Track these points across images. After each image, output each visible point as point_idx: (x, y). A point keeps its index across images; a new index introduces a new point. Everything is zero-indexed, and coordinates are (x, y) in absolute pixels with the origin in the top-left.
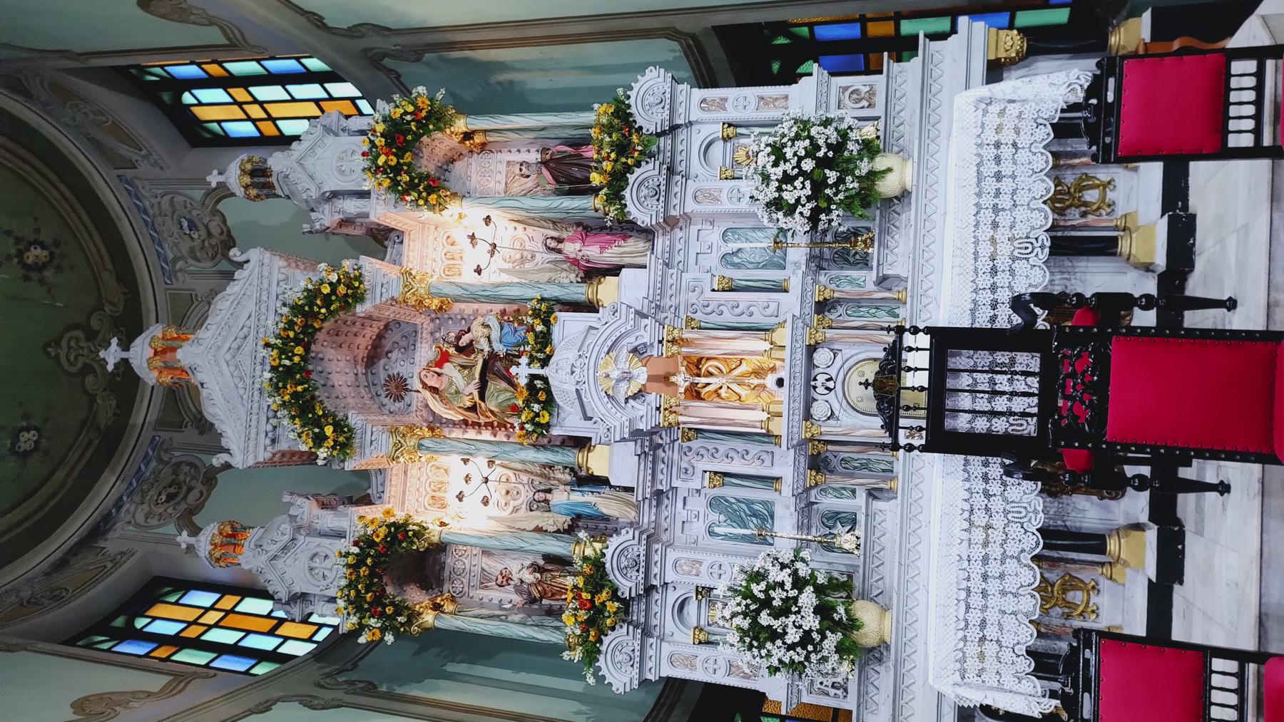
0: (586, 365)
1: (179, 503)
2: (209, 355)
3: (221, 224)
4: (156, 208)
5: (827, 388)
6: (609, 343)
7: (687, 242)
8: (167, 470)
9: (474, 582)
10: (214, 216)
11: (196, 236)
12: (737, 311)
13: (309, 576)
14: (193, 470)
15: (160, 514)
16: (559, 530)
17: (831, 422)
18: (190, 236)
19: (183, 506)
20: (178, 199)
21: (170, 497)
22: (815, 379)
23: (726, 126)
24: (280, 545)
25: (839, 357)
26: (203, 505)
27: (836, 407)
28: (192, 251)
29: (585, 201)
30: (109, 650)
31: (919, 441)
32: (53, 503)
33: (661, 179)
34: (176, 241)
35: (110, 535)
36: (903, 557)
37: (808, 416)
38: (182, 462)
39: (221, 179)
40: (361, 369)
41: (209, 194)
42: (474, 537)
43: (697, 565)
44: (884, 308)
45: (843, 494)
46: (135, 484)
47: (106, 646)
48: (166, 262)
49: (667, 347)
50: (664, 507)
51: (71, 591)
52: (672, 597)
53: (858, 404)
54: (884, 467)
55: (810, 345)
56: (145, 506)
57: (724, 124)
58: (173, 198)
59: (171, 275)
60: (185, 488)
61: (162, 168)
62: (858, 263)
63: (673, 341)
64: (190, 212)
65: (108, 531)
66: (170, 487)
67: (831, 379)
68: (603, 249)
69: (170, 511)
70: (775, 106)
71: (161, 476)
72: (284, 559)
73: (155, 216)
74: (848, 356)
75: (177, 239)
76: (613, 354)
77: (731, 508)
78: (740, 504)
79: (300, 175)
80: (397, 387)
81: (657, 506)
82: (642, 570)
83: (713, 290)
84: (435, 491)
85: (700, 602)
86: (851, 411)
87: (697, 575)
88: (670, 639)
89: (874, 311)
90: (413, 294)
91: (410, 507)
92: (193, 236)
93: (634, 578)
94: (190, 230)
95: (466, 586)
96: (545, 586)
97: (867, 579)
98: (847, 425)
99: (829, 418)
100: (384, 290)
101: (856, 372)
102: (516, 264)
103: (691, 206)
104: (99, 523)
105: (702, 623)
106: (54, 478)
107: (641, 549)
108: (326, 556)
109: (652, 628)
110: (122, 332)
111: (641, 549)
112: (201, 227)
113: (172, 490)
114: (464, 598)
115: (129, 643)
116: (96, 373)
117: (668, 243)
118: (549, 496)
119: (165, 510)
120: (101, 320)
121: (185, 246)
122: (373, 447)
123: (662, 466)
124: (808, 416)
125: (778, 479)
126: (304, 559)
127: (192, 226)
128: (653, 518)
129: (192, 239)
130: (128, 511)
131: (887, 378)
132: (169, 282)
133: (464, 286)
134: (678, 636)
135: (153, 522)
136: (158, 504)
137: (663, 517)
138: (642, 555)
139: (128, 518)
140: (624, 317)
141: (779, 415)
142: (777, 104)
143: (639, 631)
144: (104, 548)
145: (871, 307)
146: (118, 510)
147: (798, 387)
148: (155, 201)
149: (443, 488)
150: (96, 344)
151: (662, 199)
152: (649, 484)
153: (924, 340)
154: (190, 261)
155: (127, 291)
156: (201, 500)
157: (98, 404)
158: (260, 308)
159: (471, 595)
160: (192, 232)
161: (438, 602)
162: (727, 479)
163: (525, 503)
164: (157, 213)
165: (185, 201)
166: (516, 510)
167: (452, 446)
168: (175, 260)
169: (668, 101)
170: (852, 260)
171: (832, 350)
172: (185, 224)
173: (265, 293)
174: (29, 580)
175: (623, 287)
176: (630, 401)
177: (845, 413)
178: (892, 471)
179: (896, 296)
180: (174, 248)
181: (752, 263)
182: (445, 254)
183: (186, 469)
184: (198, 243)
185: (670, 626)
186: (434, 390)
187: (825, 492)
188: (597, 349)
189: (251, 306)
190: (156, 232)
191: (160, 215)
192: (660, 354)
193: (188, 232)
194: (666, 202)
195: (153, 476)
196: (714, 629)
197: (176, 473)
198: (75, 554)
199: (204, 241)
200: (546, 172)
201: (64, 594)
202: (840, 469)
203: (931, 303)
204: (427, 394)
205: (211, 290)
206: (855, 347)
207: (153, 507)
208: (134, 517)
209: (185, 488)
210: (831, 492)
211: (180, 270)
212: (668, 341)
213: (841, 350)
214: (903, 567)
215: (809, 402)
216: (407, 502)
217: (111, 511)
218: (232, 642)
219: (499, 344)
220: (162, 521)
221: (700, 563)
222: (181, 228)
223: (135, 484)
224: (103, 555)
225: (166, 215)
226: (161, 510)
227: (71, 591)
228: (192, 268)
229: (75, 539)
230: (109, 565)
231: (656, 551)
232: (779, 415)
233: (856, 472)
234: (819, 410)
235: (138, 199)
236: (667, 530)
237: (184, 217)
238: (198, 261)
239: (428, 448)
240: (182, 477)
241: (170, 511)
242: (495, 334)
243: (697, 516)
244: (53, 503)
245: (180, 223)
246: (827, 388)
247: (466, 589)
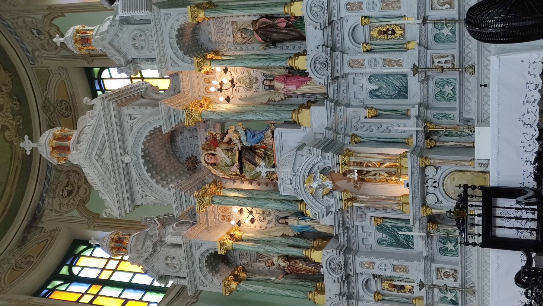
0: (298, 180)
1: (75, 196)
2: (86, 158)
3: (56, 31)
4: (15, 25)
5: (434, 187)
6: (308, 171)
7: (347, 85)
8: (62, 176)
9: (253, 259)
10: (52, 27)
11: (43, 37)
12: (382, 129)
13: (167, 268)
14: (77, 175)
15: (67, 204)
16: (295, 235)
18: (39, 37)
19: (78, 198)
20: (27, 19)
21: (70, 193)
22: (427, 182)
23: (363, 18)
24: (149, 253)
25: (439, 170)
26: (89, 196)
27: (440, 196)
28: (42, 46)
29: (284, 63)
30: (65, 291)
31: (479, 240)
32: (8, 207)
33: (328, 57)
34: (32, 41)
35: (44, 219)
36: (480, 274)
37: (424, 204)
38: (70, 171)
39: (62, 39)
40: (168, 146)
41: (46, 16)
42: (251, 247)
43: (373, 264)
46: (47, 186)
47: (63, 288)
48: (28, 52)
49: (342, 168)
50: (351, 231)
51: (35, 257)
52: (361, 279)
55: (422, 167)
56: (57, 199)
57: (362, 17)
58: (24, 19)
59: (32, 59)
60: (76, 187)
61: (14, 6)
62: (450, 100)
63: (345, 164)
64: (36, 26)
65: (41, 216)
66: (67, 186)
67: (436, 182)
68: (297, 88)
69: (71, 201)
70: (392, 7)
71: (61, 179)
72: (151, 259)
73: (16, 29)
74: (444, 170)
75: (31, 39)
76: (312, 176)
77: (389, 230)
78: (394, 228)
79: (112, 52)
80: (193, 163)
81: (347, 232)
82: (343, 269)
83: (366, 117)
84: (223, 212)
85: (376, 281)
87: (373, 269)
88: (363, 298)
90: (193, 119)
91: (211, 222)
92: (41, 38)
93: (339, 273)
94: (39, 35)
95: (249, 261)
96: (292, 267)
97: (463, 277)
99: (436, 203)
100: (176, 118)
102: (247, 85)
103: (347, 70)
104: (35, 211)
105: (379, 289)
106: (5, 193)
107: (341, 259)
108: (174, 258)
109: (352, 294)
110: (15, 99)
111: (341, 259)
112: (45, 33)
113: (69, 188)
114: (249, 267)
115: (75, 284)
116: (9, 128)
117: (336, 88)
118: (287, 221)
119: (69, 201)
120: (3, 97)
121: (38, 43)
122: (187, 204)
123: (348, 220)
124: (424, 204)
126: (162, 258)
127: (39, 32)
128: (346, 238)
129: (41, 39)
130: (48, 203)
131: (460, 210)
132: (33, 63)
133: (221, 114)
134: (366, 297)
135: (64, 209)
136: (63, 197)
137: (351, 237)
138: (342, 262)
139: (50, 207)
140: (315, 155)
141: (408, 204)
142: (393, 5)
143: (345, 298)
144: (43, 228)
146: (43, 201)
147: (417, 191)
148: (13, 21)
149: (228, 210)
150: (4, 112)
151: (329, 68)
152: (341, 225)
153: (479, 192)
154: (43, 51)
155: (11, 74)
156: (87, 194)
157: (15, 146)
158: (108, 132)
159: (253, 266)
160: (40, 36)
161: (236, 274)
162: (385, 220)
163: (274, 218)
164: (17, 27)
165: (32, 21)
166: (269, 222)
167: (230, 201)
168: (33, 51)
169: (326, 8)
170: (447, 98)
172: (35, 32)
173: (109, 124)
174: (11, 251)
175: (313, 117)
176: (325, 197)
180: (31, 44)
181: (388, 95)
182: (204, 80)
183: (73, 174)
184: (45, 41)
185: (361, 292)
186: (213, 164)
188: (303, 171)
189: (103, 130)
190: (18, 36)
191: (18, 28)
192: (338, 171)
193: (37, 36)
194: (332, 70)
195: (56, 180)
196: (385, 292)
197: (68, 177)
198: (29, 232)
199: (48, 40)
200: (256, 35)
201: (32, 260)
204: (210, 167)
205: (59, 67)
207: (61, 200)
208: (52, 206)
209: (76, 187)
211: (38, 56)
212: (342, 164)
214: (480, 279)
215: (424, 195)
216: (209, 220)
217: (39, 203)
218: (127, 280)
219: (246, 143)
220: (69, 209)
221: (374, 263)
222: (33, 34)
223: (47, 186)
224: (44, 232)
225: (22, 28)
226: (66, 202)
227: (35, 257)
228: (44, 55)
229: (25, 223)
230: (50, 239)
231: (350, 258)
232: (408, 204)
234: (431, 200)
235: (3, 20)
236: (354, 243)
237: (33, 28)
238: (47, 51)
239: (218, 203)
240: (72, 180)
241: (71, 201)
242: (243, 138)
243: (370, 235)
244: (8, 207)
245: (32, 31)
246: (434, 187)
247: (249, 263)
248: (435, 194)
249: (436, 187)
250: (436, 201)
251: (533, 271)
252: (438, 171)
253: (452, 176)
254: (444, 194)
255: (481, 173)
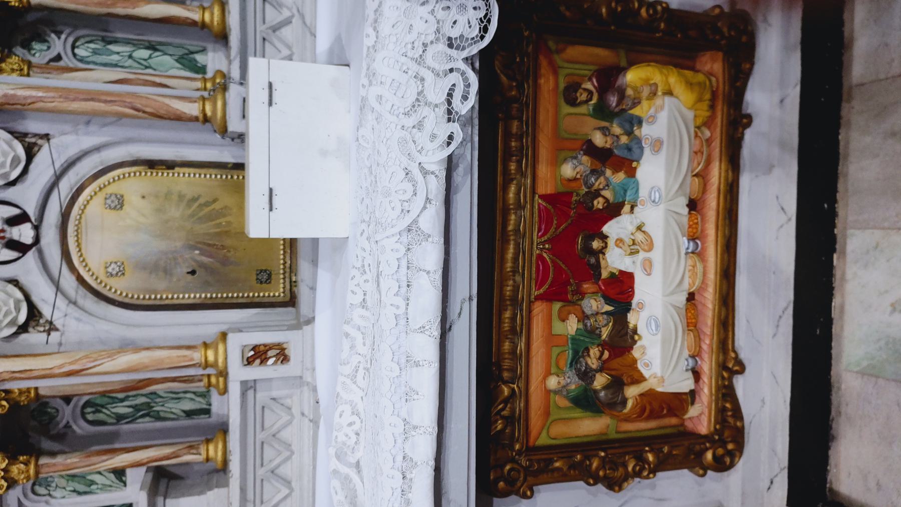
17: (35, 337)
25: (42, 158)
27: (43, 294)
44: (171, 50)
45: (93, 483)
53: (112, 282)
54: (188, 406)
67: (21, 218)
86: (89, 302)
89: (143, 53)
98: (80, 344)
99: (23, 329)
101: (100, 197)
125: (280, 51)
145: (137, 44)
171: (20, 136)
177: (72, 309)
178: (207, 412)
179: (196, 16)
187: (48, 486)
202: (81, 428)
203: (287, 22)
206: (92, 128)
210: (63, 482)
213: (47, 137)
233: (125, 427)
248: (15, 282)
249: (21, 248)
250: (22, 317)
251: (528, 463)
252: (37, 160)
253: (110, 190)
254: (68, 282)
255: (459, 312)
